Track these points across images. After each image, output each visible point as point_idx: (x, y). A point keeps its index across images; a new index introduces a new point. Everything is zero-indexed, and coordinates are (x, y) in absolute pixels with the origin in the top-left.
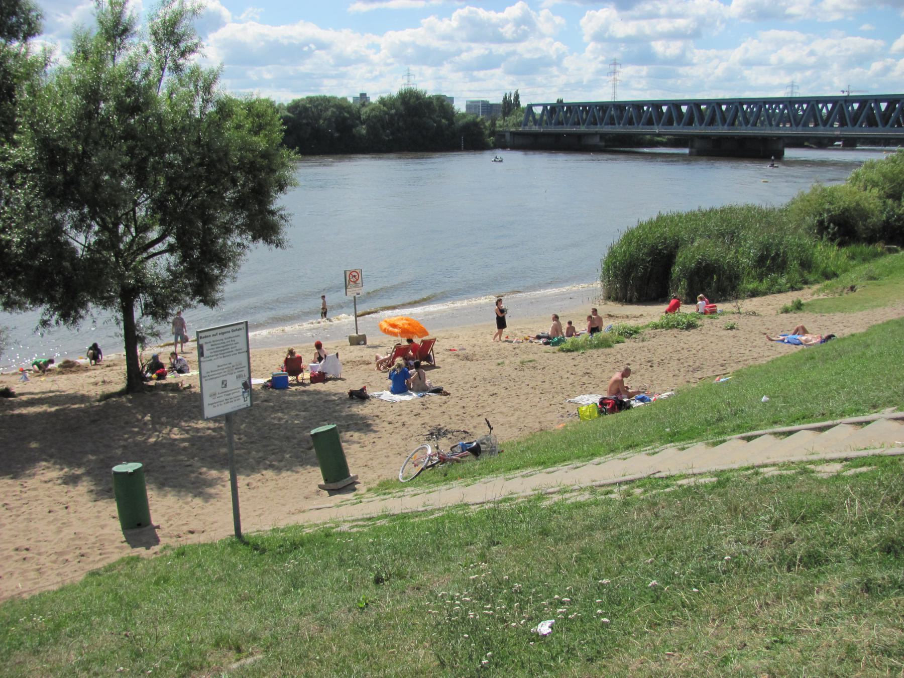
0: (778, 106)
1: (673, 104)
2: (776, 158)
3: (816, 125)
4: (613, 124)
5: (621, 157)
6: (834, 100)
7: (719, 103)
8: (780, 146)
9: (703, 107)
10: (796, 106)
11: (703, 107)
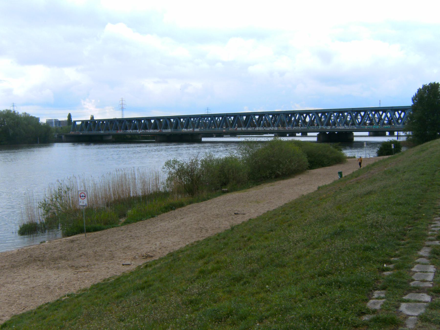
0: (207, 118)
1: (157, 119)
2: (325, 133)
3: (215, 127)
4: (109, 130)
5: (143, 145)
6: (222, 115)
7: (179, 117)
8: (200, 138)
9: (172, 120)
10: (217, 118)
11: (161, 120)
